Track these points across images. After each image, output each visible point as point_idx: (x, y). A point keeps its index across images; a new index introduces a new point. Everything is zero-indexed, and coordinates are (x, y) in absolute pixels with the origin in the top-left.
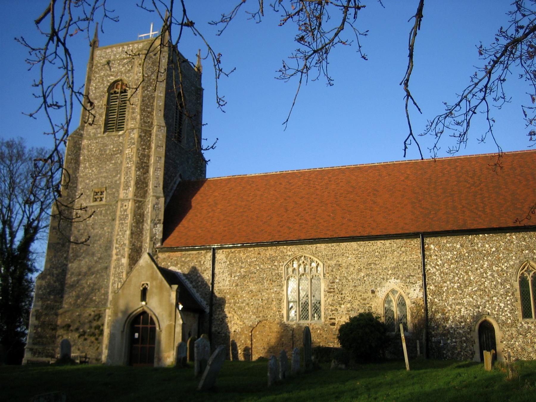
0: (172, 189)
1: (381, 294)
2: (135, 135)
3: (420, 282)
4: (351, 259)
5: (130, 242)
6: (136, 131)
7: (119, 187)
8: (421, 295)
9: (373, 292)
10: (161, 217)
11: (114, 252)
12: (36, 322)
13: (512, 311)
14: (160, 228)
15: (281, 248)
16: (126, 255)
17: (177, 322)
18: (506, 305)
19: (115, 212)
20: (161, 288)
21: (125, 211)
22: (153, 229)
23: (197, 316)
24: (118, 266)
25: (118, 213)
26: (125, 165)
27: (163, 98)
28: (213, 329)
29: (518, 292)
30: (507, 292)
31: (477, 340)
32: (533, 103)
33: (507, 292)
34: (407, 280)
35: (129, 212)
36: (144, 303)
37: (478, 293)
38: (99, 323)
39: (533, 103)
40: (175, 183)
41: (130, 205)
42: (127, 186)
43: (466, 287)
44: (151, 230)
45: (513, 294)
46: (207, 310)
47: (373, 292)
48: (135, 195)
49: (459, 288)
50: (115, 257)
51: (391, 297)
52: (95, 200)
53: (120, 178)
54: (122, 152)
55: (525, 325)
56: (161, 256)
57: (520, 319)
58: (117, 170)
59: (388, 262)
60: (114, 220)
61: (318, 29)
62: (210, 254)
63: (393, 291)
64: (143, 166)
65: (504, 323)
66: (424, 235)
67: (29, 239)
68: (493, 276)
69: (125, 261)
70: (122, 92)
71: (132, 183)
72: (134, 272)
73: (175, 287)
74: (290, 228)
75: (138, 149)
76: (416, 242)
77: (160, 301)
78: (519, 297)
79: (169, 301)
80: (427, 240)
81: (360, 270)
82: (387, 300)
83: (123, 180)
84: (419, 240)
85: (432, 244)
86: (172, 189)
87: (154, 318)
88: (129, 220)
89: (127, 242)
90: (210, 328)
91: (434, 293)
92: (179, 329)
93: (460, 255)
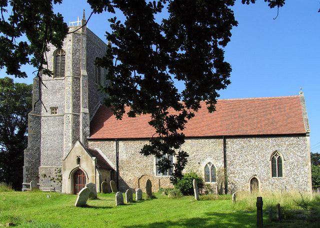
0: (96, 109)
2: (70, 80)
5: (73, 135)
6: (71, 78)
9: (199, 163)
10: (89, 123)
11: (65, 140)
14: (88, 129)
17: (97, 175)
20: (87, 158)
21: (69, 119)
22: (83, 129)
26: (66, 96)
27: (85, 60)
34: (217, 159)
35: (70, 120)
36: (78, 165)
37: (252, 165)
38: (61, 174)
40: (98, 106)
43: (245, 162)
44: (83, 130)
47: (199, 163)
48: (73, 112)
50: (65, 143)
51: (208, 165)
55: (273, 180)
56: (90, 143)
64: (76, 97)
70: (62, 56)
71: (33, 106)
73: (94, 158)
75: (73, 88)
76: (222, 140)
77: (87, 165)
79: (92, 164)
80: (227, 140)
84: (115, 143)
85: (121, 143)
86: (96, 109)
87: (85, 173)
89: (71, 135)
92: (98, 178)
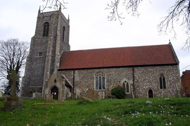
1: (122, 82)
2: (52, 38)
3: (132, 79)
4: (113, 73)
7: (47, 52)
8: (133, 82)
9: (119, 82)
10: (59, 61)
11: (45, 70)
12: (22, 91)
13: (157, 87)
15: (94, 70)
16: (49, 72)
18: (156, 85)
19: (45, 59)
21: (48, 59)
23: (70, 88)
24: (47, 74)
25: (46, 60)
28: (74, 92)
29: (159, 82)
30: (156, 82)
31: (148, 95)
32: (162, 75)
33: (156, 82)
34: (129, 79)
39: (162, 75)
41: (50, 57)
42: (49, 52)
43: (145, 80)
45: (158, 83)
46: (72, 87)
47: (119, 82)
49: (143, 81)
50: (45, 72)
52: (40, 56)
53: (47, 50)
54: (47, 42)
57: (160, 89)
58: (46, 48)
59: (124, 73)
60: (45, 62)
61: (19, 61)
62: (73, 71)
63: (125, 82)
65: (155, 90)
66: (133, 67)
67: (18, 68)
68: (152, 78)
69: (48, 73)
71: (51, 51)
72: (52, 76)
74: (96, 64)
76: (131, 68)
78: (159, 83)
81: (116, 76)
82: (124, 84)
83: (48, 50)
88: (50, 62)
90: (73, 92)
91: (136, 82)
93: (144, 72)
